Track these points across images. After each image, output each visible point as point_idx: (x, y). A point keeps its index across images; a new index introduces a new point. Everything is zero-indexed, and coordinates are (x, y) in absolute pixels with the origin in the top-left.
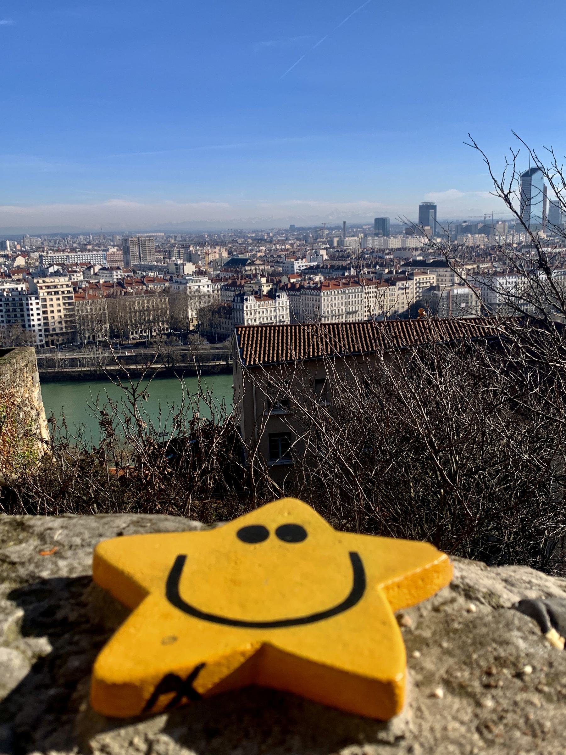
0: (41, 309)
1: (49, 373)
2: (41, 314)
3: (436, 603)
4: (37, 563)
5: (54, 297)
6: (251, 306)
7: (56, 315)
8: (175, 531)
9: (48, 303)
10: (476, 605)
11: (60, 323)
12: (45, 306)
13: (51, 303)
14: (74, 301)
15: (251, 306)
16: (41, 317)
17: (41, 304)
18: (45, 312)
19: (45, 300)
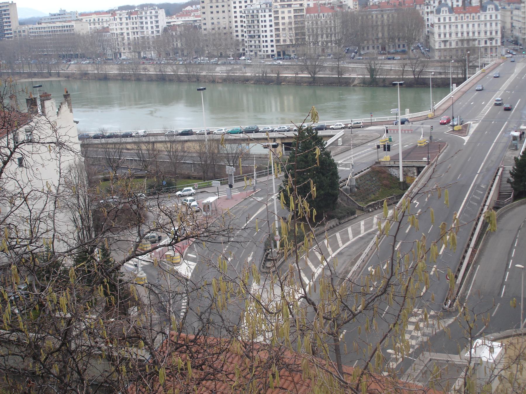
0: (273, 21)
1: (272, 77)
2: (273, 25)
3: (487, 380)
4: (412, 336)
5: (286, 10)
6: (445, 19)
7: (287, 20)
8: (90, 14)
9: (280, 15)
10: (132, 261)
11: (290, 23)
12: (277, 18)
13: (283, 15)
14: (305, 14)
15: (445, 19)
16: (273, 28)
17: (273, 16)
18: (277, 24)
19: (276, 12)
